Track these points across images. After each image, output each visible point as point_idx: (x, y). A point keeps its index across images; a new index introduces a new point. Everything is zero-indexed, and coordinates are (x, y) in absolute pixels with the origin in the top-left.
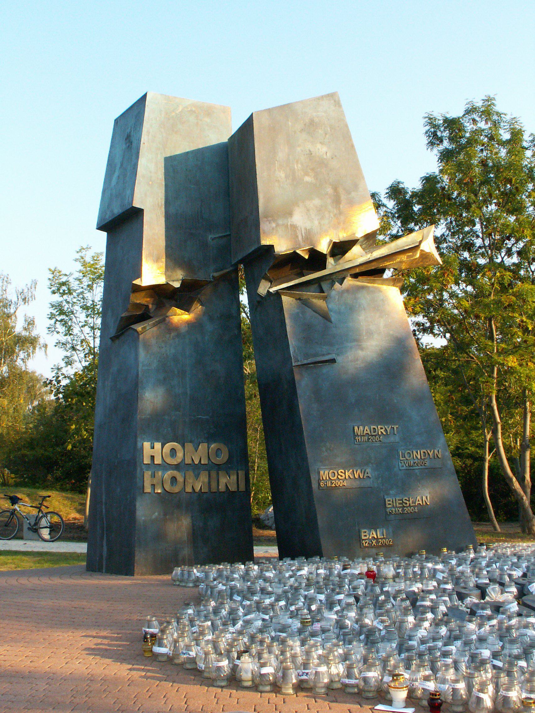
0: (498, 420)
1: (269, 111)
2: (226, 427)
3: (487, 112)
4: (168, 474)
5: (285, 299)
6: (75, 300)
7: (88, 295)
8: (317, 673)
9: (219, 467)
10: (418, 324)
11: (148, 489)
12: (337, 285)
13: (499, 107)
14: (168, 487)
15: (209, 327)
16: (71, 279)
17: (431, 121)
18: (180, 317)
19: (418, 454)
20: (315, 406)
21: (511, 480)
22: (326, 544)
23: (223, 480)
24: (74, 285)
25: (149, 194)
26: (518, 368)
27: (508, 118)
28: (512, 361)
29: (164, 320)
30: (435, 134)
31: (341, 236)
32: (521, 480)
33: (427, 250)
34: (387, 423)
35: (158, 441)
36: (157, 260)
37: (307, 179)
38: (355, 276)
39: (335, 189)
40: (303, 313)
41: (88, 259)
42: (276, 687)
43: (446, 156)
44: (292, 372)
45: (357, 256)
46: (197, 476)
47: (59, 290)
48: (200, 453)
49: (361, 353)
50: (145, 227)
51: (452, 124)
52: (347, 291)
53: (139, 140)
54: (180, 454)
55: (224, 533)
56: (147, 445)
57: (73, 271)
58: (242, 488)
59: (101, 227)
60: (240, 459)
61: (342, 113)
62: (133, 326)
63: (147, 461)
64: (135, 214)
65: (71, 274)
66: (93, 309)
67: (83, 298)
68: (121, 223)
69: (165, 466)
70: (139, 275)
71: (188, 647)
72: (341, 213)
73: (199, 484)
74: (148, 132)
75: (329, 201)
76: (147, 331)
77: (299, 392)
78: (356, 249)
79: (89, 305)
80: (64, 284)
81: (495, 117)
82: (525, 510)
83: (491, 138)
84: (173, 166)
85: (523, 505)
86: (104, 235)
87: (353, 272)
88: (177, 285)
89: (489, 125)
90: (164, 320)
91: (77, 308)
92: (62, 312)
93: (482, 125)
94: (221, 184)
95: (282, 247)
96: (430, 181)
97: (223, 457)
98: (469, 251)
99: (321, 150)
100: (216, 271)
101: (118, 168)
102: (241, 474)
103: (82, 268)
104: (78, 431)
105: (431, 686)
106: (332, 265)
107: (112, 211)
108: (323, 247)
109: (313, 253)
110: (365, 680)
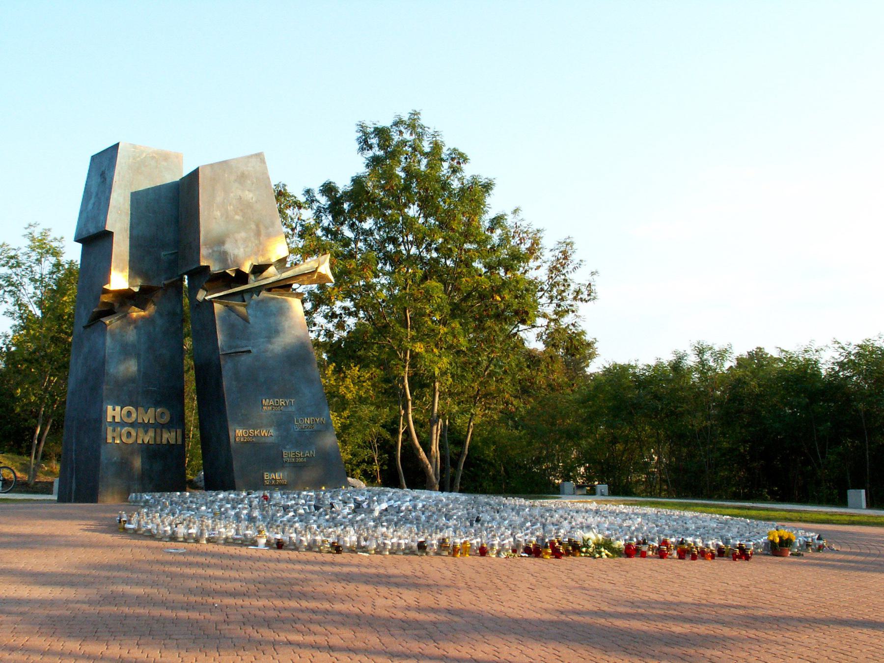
0: (409, 397)
1: (212, 165)
2: (168, 396)
3: (413, 124)
4: (125, 430)
5: (217, 307)
6: (23, 273)
7: (37, 268)
8: (219, 532)
9: (163, 426)
10: (344, 308)
11: (110, 440)
12: (255, 296)
13: (424, 121)
14: (124, 439)
15: (159, 322)
16: (19, 253)
17: (362, 128)
18: (136, 313)
19: (308, 421)
20: (234, 383)
21: (418, 450)
22: (238, 482)
23: (166, 436)
24: (22, 258)
25: (118, 221)
26: (424, 353)
27: (431, 131)
28: (419, 348)
29: (125, 316)
30: (366, 141)
31: (261, 260)
32: (428, 451)
33: (323, 272)
34: (287, 397)
35: (118, 405)
36: (122, 270)
37: (237, 217)
38: (269, 290)
39: (257, 226)
40: (229, 316)
41: (37, 235)
42: (197, 540)
43: (375, 161)
44: (219, 359)
45: (272, 274)
46: (146, 432)
47: (8, 263)
48: (149, 416)
49: (271, 347)
50: (114, 245)
51: (382, 133)
52: (262, 301)
53: (112, 179)
54: (134, 415)
55: (164, 472)
56: (110, 408)
57: (22, 246)
58: (180, 442)
59: (77, 240)
60: (178, 421)
61: (266, 168)
62: (103, 319)
63: (109, 419)
64: (108, 236)
65: (19, 249)
66: (41, 282)
67: (32, 272)
68: (95, 240)
69: (123, 424)
70: (108, 281)
71: (147, 523)
72: (260, 244)
73: (147, 438)
74: (119, 173)
75: (252, 234)
76: (112, 323)
77: (224, 373)
78: (272, 270)
79: (37, 277)
80: (12, 258)
81: (420, 130)
82: (430, 478)
83: (415, 149)
84: (136, 198)
85: (428, 472)
86: (80, 246)
87: (268, 287)
88: (136, 289)
89: (414, 137)
90: (125, 316)
91: (26, 280)
92: (11, 284)
93: (407, 136)
94: (174, 209)
95: (215, 268)
96: (357, 181)
97: (166, 419)
98: (394, 244)
99: (249, 196)
100: (166, 279)
101: (93, 197)
102: (179, 431)
103: (30, 243)
104: (26, 394)
105: (279, 536)
106: (253, 283)
107: (87, 230)
108: (246, 269)
109: (239, 272)
110: (245, 535)
